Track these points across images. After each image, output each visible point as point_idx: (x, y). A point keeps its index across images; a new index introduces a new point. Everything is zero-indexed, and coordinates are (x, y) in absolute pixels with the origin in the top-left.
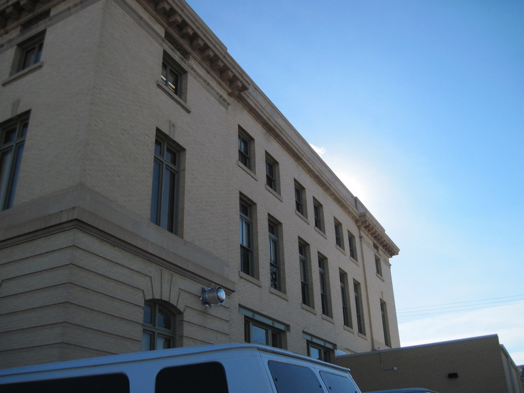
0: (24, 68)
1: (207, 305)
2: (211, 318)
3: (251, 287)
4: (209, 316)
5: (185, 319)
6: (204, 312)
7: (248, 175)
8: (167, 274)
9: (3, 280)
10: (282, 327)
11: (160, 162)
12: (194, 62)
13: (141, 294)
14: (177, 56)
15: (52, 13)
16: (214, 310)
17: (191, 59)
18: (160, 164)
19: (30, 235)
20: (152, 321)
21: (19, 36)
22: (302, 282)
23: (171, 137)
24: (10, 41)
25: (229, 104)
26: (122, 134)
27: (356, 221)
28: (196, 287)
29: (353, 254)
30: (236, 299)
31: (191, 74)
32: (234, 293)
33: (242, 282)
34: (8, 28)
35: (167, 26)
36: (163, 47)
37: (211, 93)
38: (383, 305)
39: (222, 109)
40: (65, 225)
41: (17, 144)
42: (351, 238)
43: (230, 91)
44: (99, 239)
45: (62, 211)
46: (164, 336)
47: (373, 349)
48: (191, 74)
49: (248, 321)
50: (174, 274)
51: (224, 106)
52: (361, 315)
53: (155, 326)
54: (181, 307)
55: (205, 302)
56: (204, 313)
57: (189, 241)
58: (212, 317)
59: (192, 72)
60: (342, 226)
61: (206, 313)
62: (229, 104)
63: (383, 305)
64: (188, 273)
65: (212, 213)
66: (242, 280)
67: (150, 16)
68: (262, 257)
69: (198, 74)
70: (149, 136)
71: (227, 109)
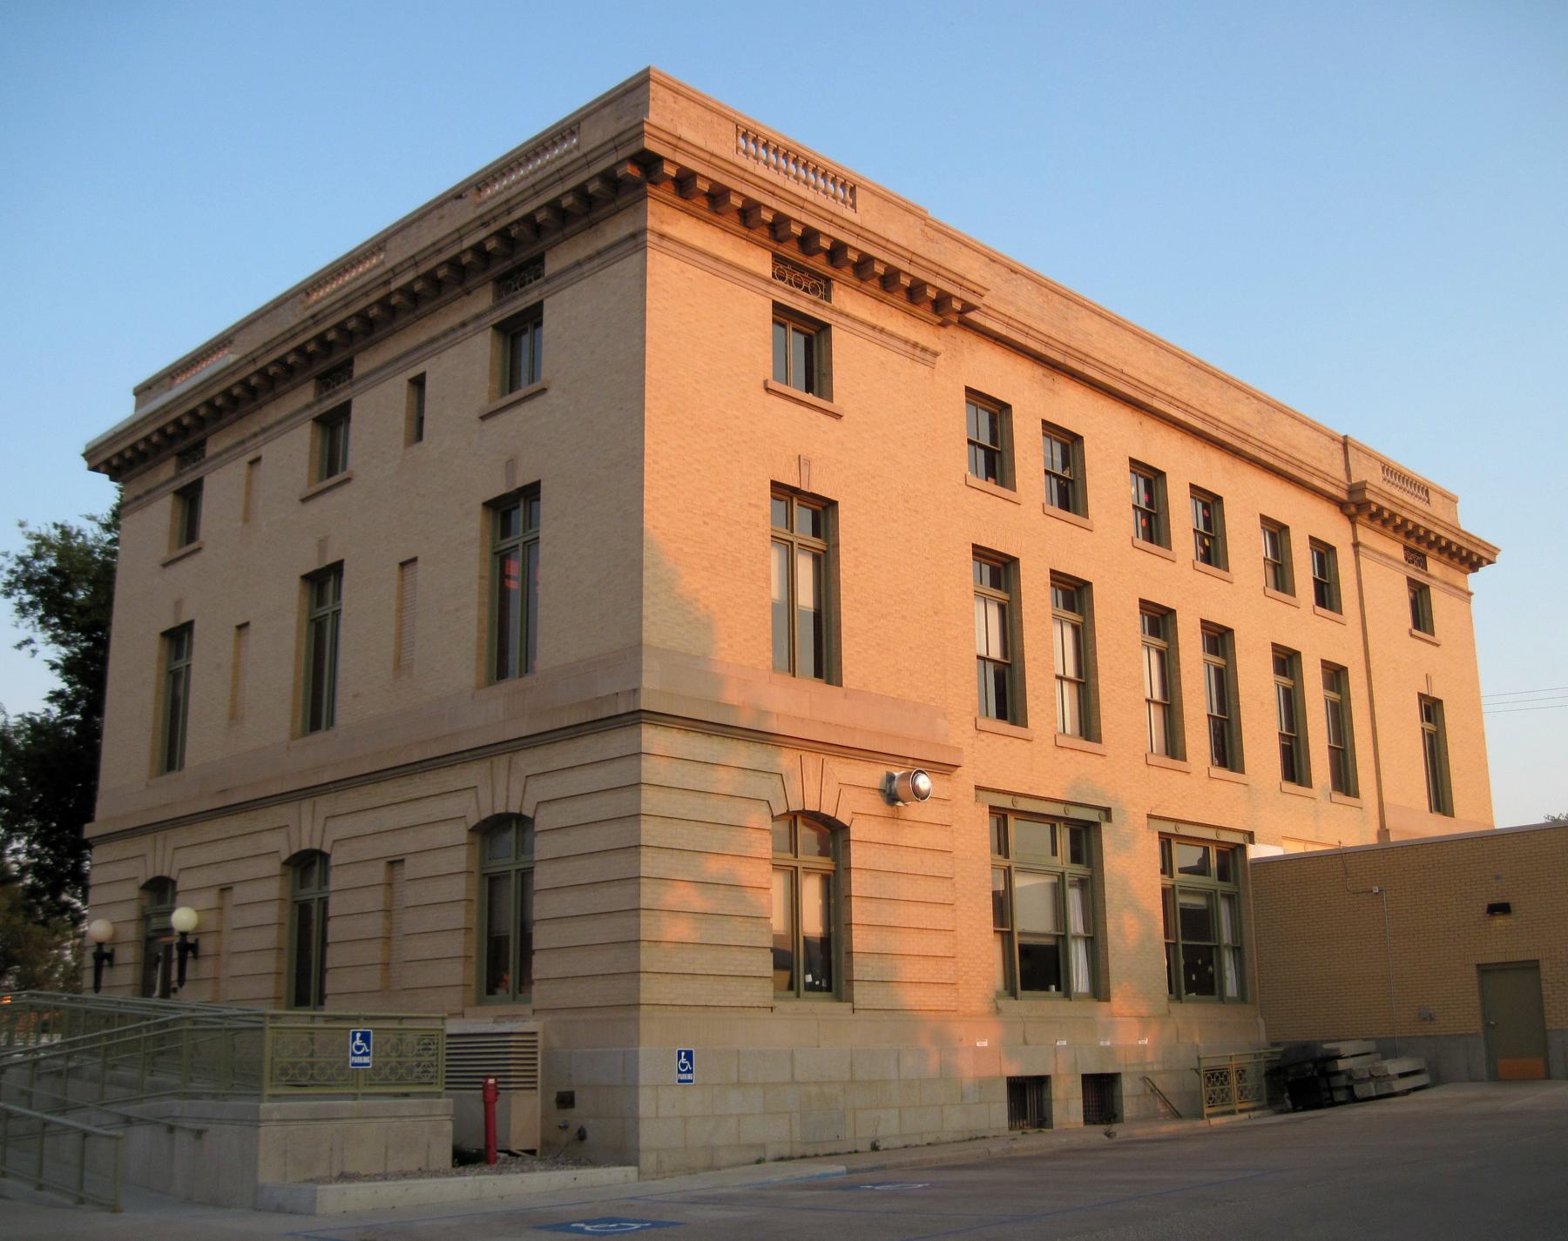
0: (511, 391)
1: (900, 804)
2: (909, 826)
3: (1006, 745)
4: (905, 823)
5: (851, 838)
6: (894, 818)
7: (994, 497)
8: (811, 762)
9: (538, 803)
10: (1092, 816)
11: (788, 543)
12: (845, 292)
13: (765, 809)
14: (802, 303)
15: (551, 267)
16: (913, 810)
17: (836, 290)
18: (788, 546)
19: (572, 730)
20: (794, 848)
21: (493, 309)
22: (1315, 579)
23: (804, 488)
24: (478, 317)
25: (936, 354)
26: (705, 523)
27: (1341, 505)
28: (874, 775)
29: (1326, 595)
30: (967, 778)
31: (839, 325)
32: (959, 768)
33: (982, 741)
34: (468, 284)
35: (774, 245)
36: (769, 295)
37: (891, 348)
38: (1431, 709)
39: (921, 370)
40: (625, 718)
41: (525, 543)
42: (1324, 553)
43: (939, 320)
44: (682, 731)
45: (617, 694)
46: (818, 871)
47: (1383, 832)
48: (839, 325)
49: (1000, 816)
50: (827, 758)
51: (924, 362)
52: (1348, 747)
53: (796, 856)
54: (843, 818)
55: (891, 798)
56: (895, 818)
57: (855, 688)
58: (910, 823)
59: (842, 320)
60: (1289, 532)
61: (898, 818)
62: (936, 354)
63: (1431, 709)
64: (853, 751)
65: (903, 617)
66: (983, 736)
67: (737, 239)
68: (1035, 673)
69: (854, 319)
70: (756, 506)
71: (932, 366)
